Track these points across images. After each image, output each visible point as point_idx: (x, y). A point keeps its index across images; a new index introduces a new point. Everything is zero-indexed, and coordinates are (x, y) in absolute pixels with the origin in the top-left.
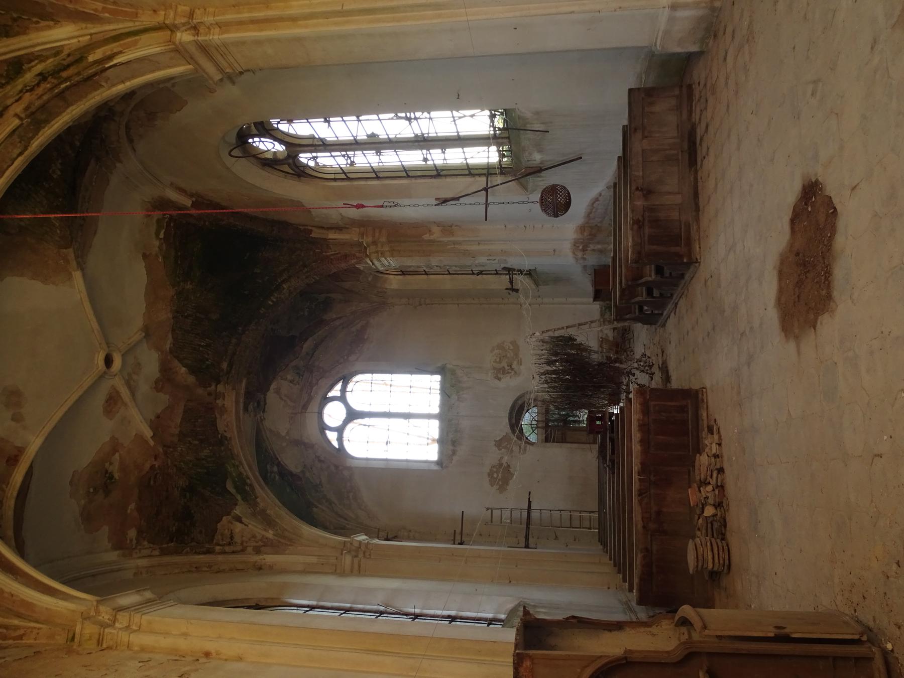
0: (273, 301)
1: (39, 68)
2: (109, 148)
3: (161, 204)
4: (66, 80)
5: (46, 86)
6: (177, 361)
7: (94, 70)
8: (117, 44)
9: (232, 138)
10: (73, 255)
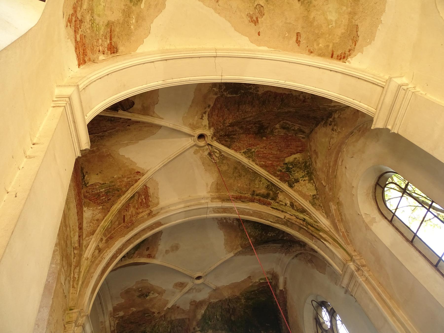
1: (307, 218)
2: (289, 249)
3: (275, 277)
4: (307, 228)
5: (302, 222)
7: (317, 236)
8: (333, 241)
9: (320, 300)
10: (239, 250)
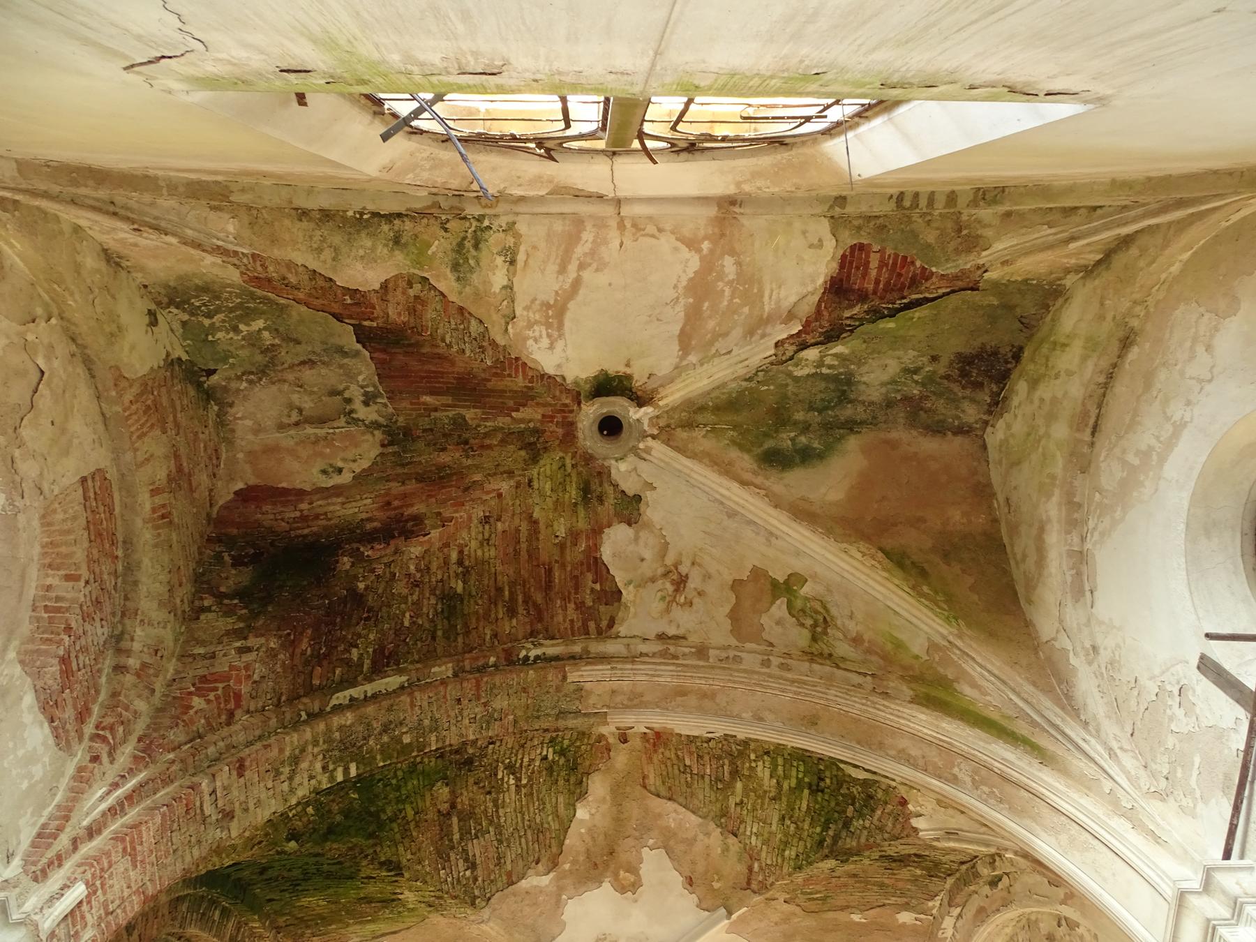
0: (346, 770)
6: (567, 842)
